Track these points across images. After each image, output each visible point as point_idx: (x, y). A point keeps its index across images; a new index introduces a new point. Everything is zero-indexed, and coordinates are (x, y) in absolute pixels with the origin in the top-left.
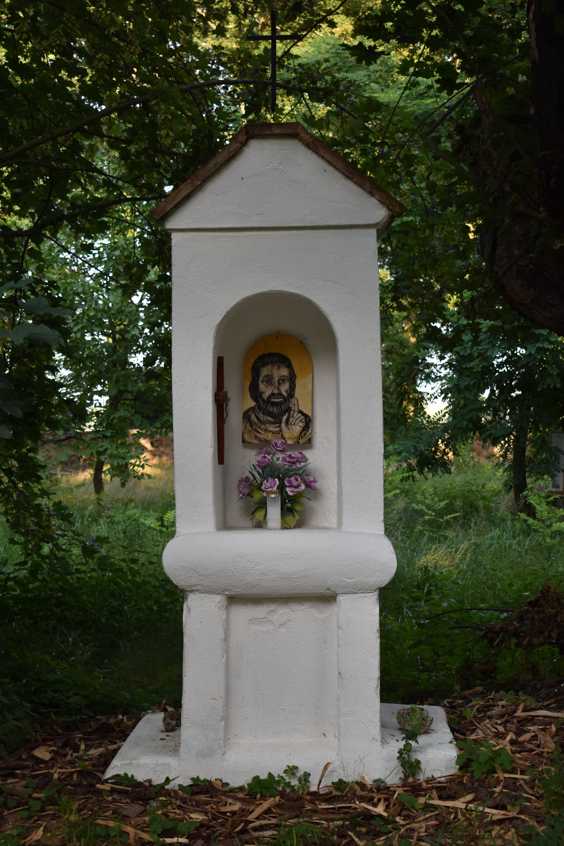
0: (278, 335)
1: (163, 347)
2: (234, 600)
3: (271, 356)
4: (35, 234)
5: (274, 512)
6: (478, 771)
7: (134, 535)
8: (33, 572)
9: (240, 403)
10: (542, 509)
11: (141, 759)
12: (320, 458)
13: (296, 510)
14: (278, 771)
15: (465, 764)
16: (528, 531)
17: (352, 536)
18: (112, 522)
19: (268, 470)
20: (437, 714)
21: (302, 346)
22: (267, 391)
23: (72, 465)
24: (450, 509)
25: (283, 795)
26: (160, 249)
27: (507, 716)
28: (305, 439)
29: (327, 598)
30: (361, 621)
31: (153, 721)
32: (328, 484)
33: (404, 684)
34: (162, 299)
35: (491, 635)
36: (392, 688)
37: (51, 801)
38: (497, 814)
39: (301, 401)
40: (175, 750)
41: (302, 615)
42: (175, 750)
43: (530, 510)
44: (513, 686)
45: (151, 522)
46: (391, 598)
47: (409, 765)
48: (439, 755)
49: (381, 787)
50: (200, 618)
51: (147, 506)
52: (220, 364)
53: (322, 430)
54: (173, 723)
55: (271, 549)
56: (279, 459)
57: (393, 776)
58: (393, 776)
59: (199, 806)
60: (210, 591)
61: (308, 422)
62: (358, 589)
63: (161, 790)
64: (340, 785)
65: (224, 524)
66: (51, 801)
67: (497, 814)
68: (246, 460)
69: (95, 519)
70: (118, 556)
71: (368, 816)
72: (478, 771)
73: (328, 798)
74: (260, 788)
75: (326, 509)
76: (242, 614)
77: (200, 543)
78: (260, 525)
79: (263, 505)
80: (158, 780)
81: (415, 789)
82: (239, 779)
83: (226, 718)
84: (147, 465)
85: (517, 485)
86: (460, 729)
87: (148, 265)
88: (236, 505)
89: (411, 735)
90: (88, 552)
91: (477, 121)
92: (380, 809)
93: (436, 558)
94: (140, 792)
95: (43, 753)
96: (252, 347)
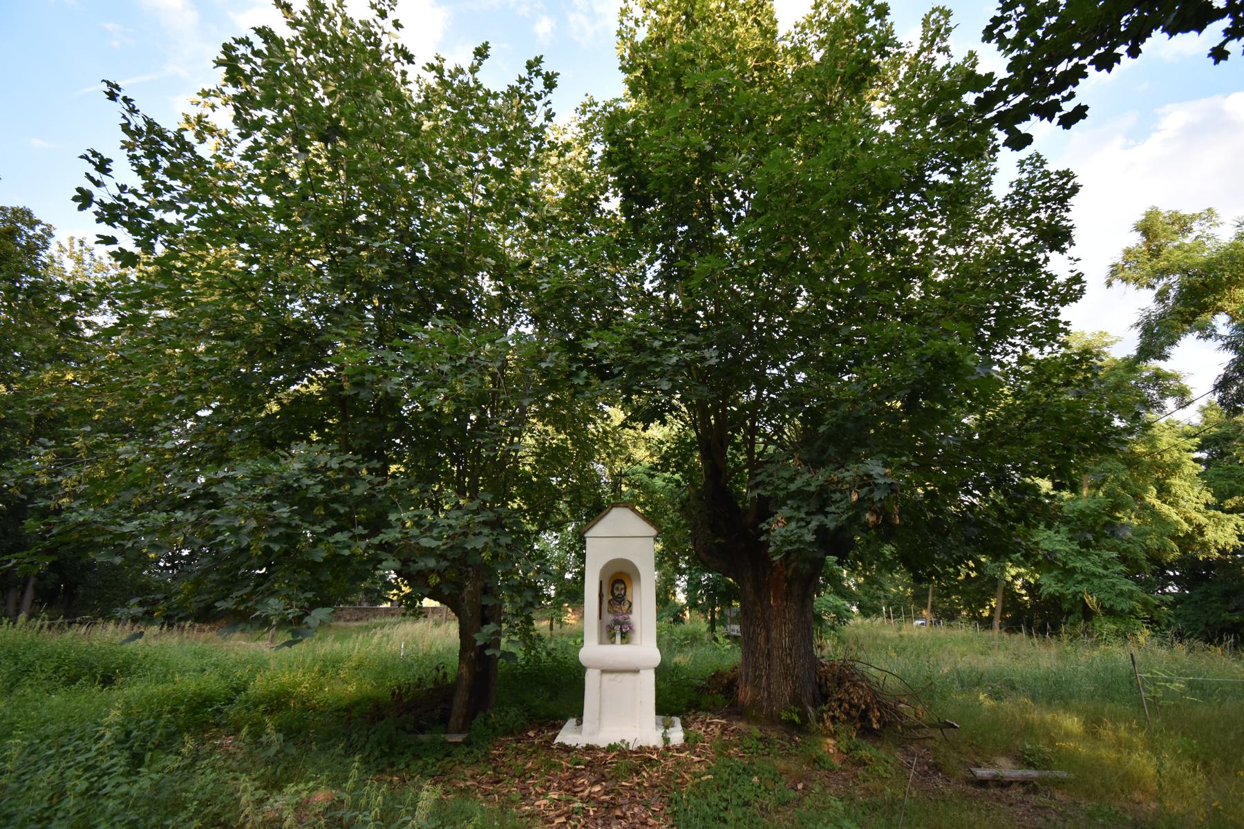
0: (621, 573)
1: (582, 573)
2: (603, 671)
3: (619, 581)
4: (538, 533)
5: (618, 638)
6: (691, 741)
7: (566, 648)
8: (527, 662)
9: (606, 598)
10: (721, 639)
11: (568, 736)
12: (634, 618)
13: (626, 637)
14: (618, 742)
15: (686, 739)
16: (715, 649)
17: (645, 648)
18: (556, 643)
19: (617, 622)
20: (677, 720)
21: (629, 577)
22: (617, 593)
23: (542, 619)
24: (686, 639)
25: (619, 751)
26: (580, 538)
27: (702, 722)
28: (629, 611)
29: (636, 671)
30: (647, 684)
31: (572, 722)
32: (637, 627)
33: (666, 708)
34: (582, 557)
35: (699, 690)
36: (660, 710)
37: (534, 752)
38: (697, 759)
39: (628, 597)
40: (580, 732)
41: (627, 677)
42: (580, 732)
43: (716, 639)
44: (707, 710)
45: (572, 643)
46: (660, 672)
47: (666, 740)
48: (677, 736)
49: (655, 748)
50: (591, 678)
51: (570, 636)
52: (601, 583)
53: (635, 608)
54: (580, 722)
55: (617, 652)
56: (620, 618)
57: (660, 744)
58: (660, 745)
59: (588, 755)
60: (595, 668)
61: (631, 604)
62: (647, 668)
63: (575, 748)
64: (640, 747)
65: (601, 643)
66: (534, 752)
67: (697, 759)
68: (609, 618)
69: (550, 640)
70: (559, 656)
71: (651, 759)
72: (691, 741)
73: (636, 752)
74: (611, 748)
75: (637, 637)
76: (607, 677)
77: (592, 651)
78: (613, 643)
79: (614, 635)
80: (574, 744)
81: (668, 749)
82: (604, 745)
83: (600, 719)
84: (570, 618)
85: (712, 629)
86: (685, 726)
87: (578, 545)
88: (605, 635)
89: (667, 727)
90: (549, 654)
91: (688, 500)
92: (655, 757)
93: (680, 659)
94: (567, 749)
95: (531, 734)
96: (613, 576)
